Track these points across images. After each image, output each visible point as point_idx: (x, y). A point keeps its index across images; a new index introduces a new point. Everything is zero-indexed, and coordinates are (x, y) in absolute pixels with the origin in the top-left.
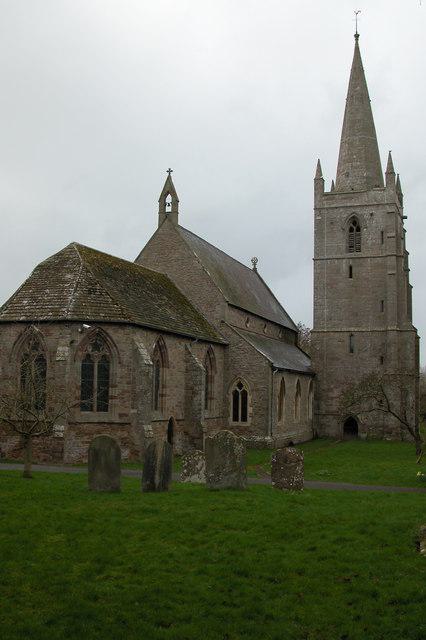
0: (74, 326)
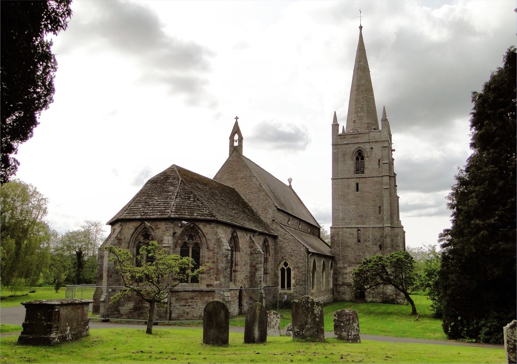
0: (176, 222)
